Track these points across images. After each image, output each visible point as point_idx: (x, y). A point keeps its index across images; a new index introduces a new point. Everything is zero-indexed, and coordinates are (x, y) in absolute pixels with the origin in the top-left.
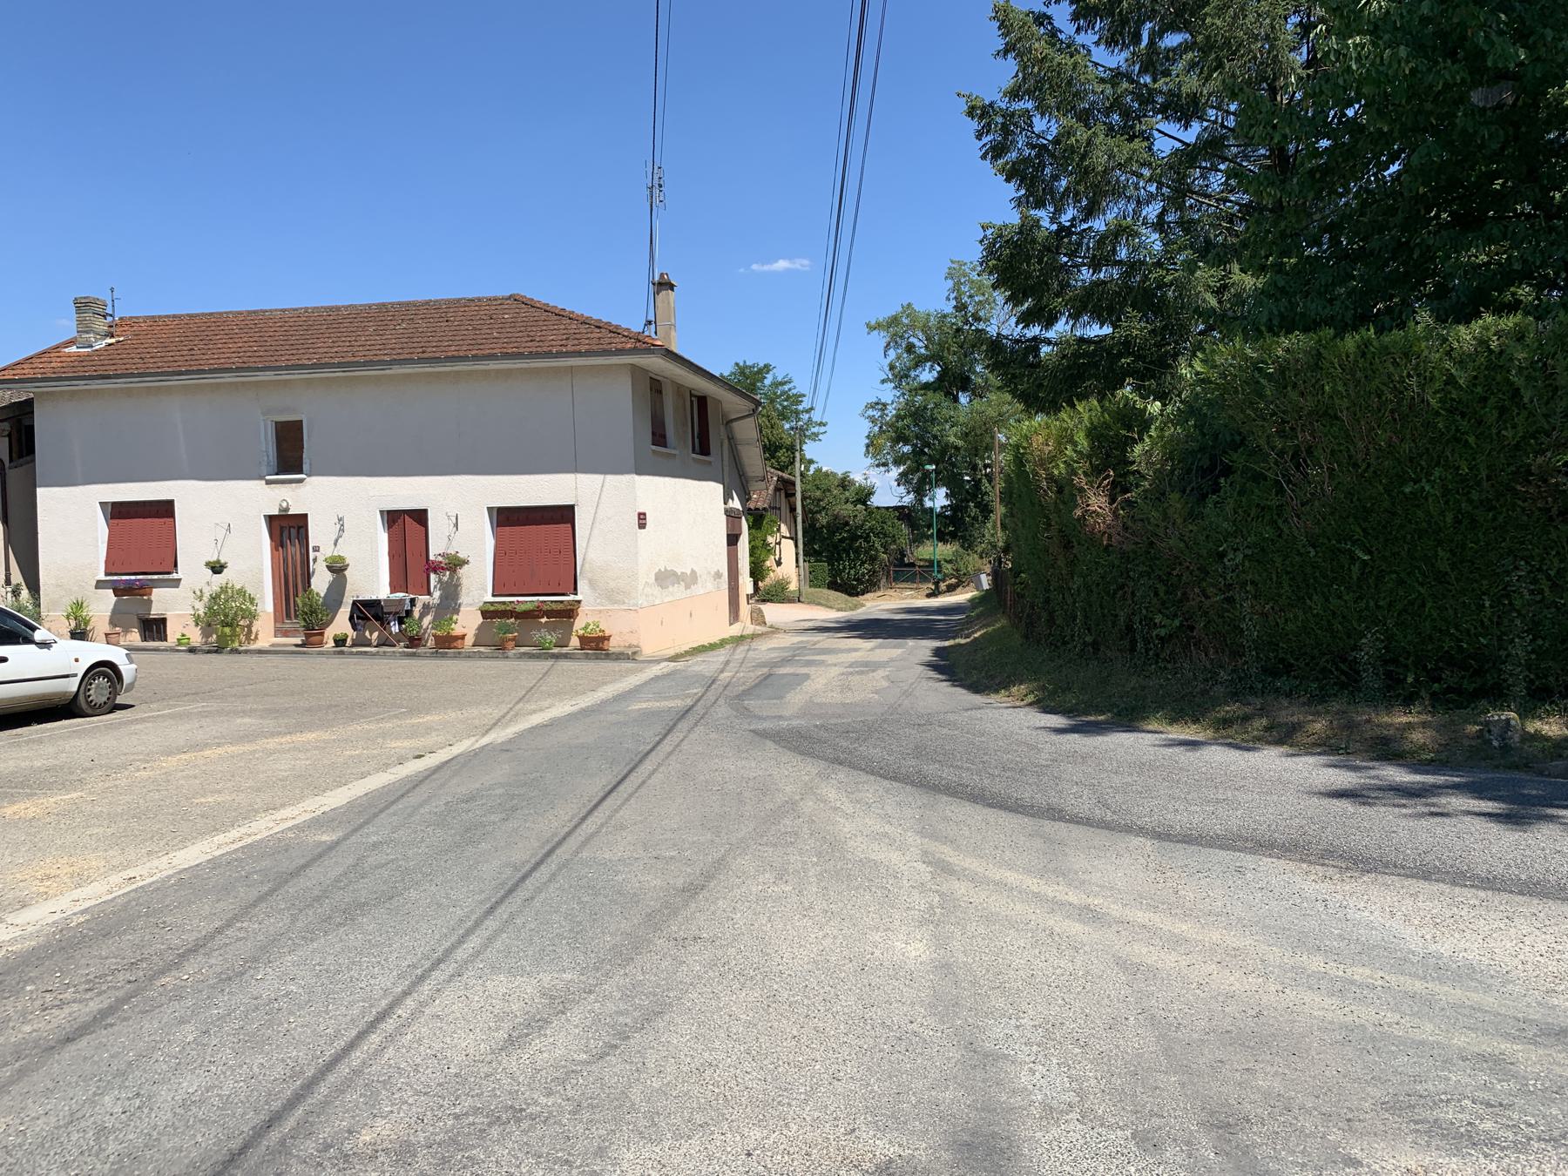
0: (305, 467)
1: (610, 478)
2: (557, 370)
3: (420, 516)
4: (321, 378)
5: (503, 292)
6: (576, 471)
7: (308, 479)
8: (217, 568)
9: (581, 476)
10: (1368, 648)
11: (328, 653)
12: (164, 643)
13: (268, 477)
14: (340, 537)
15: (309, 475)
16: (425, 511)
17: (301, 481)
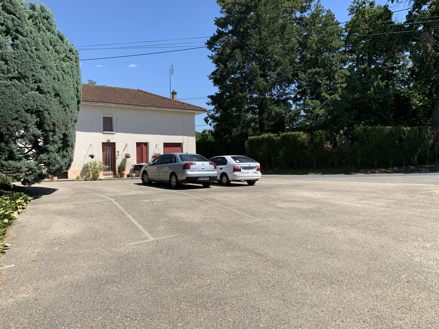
0: (115, 130)
1: (190, 137)
2: (179, 112)
3: (146, 144)
4: (127, 107)
5: (136, 88)
6: (183, 135)
7: (116, 133)
8: (92, 157)
9: (184, 137)
10: (376, 162)
11: (126, 179)
12: (67, 179)
13: (104, 132)
14: (125, 149)
15: (116, 132)
16: (137, 143)
17: (114, 133)
